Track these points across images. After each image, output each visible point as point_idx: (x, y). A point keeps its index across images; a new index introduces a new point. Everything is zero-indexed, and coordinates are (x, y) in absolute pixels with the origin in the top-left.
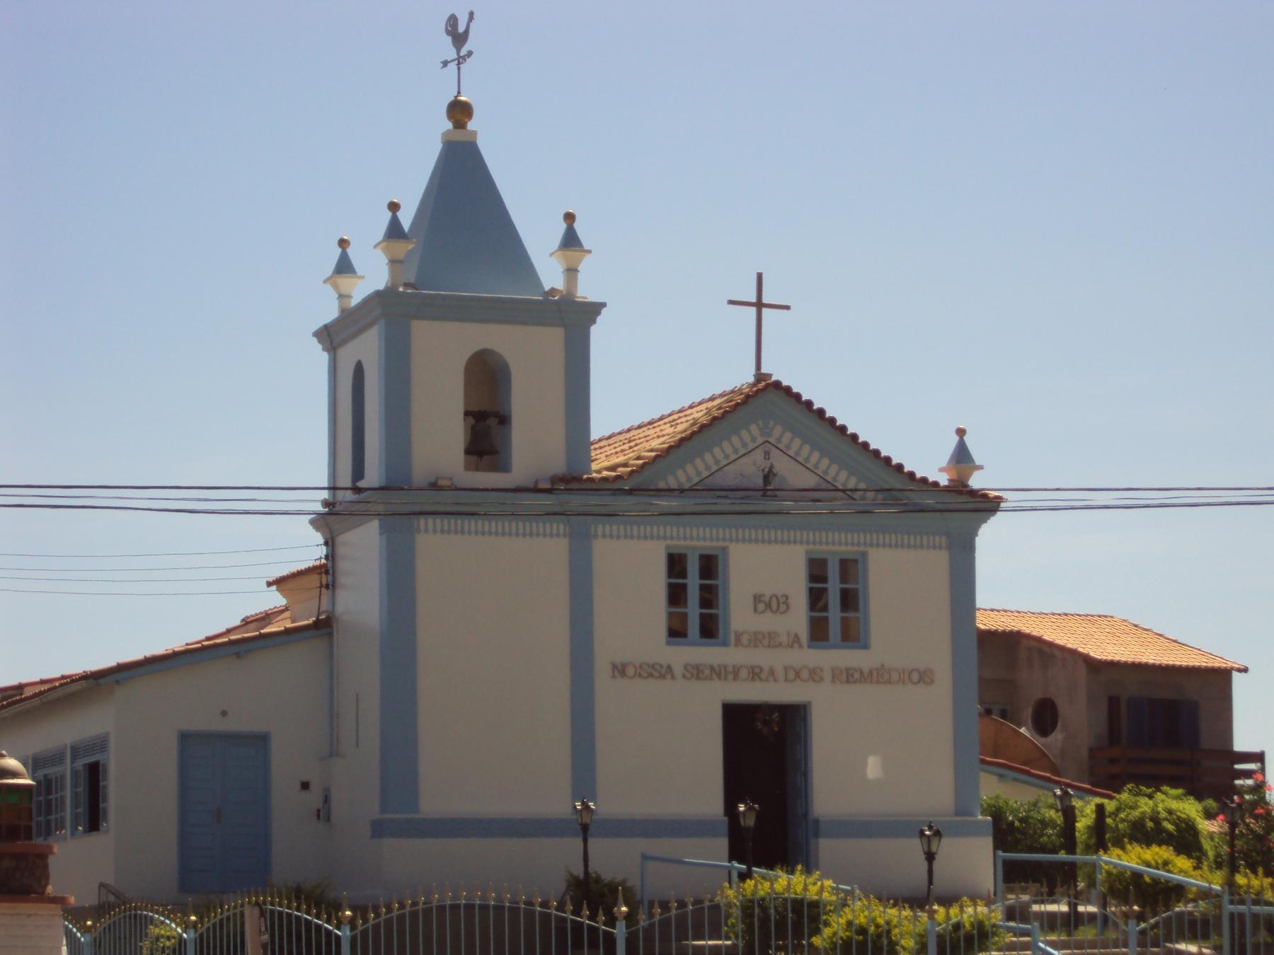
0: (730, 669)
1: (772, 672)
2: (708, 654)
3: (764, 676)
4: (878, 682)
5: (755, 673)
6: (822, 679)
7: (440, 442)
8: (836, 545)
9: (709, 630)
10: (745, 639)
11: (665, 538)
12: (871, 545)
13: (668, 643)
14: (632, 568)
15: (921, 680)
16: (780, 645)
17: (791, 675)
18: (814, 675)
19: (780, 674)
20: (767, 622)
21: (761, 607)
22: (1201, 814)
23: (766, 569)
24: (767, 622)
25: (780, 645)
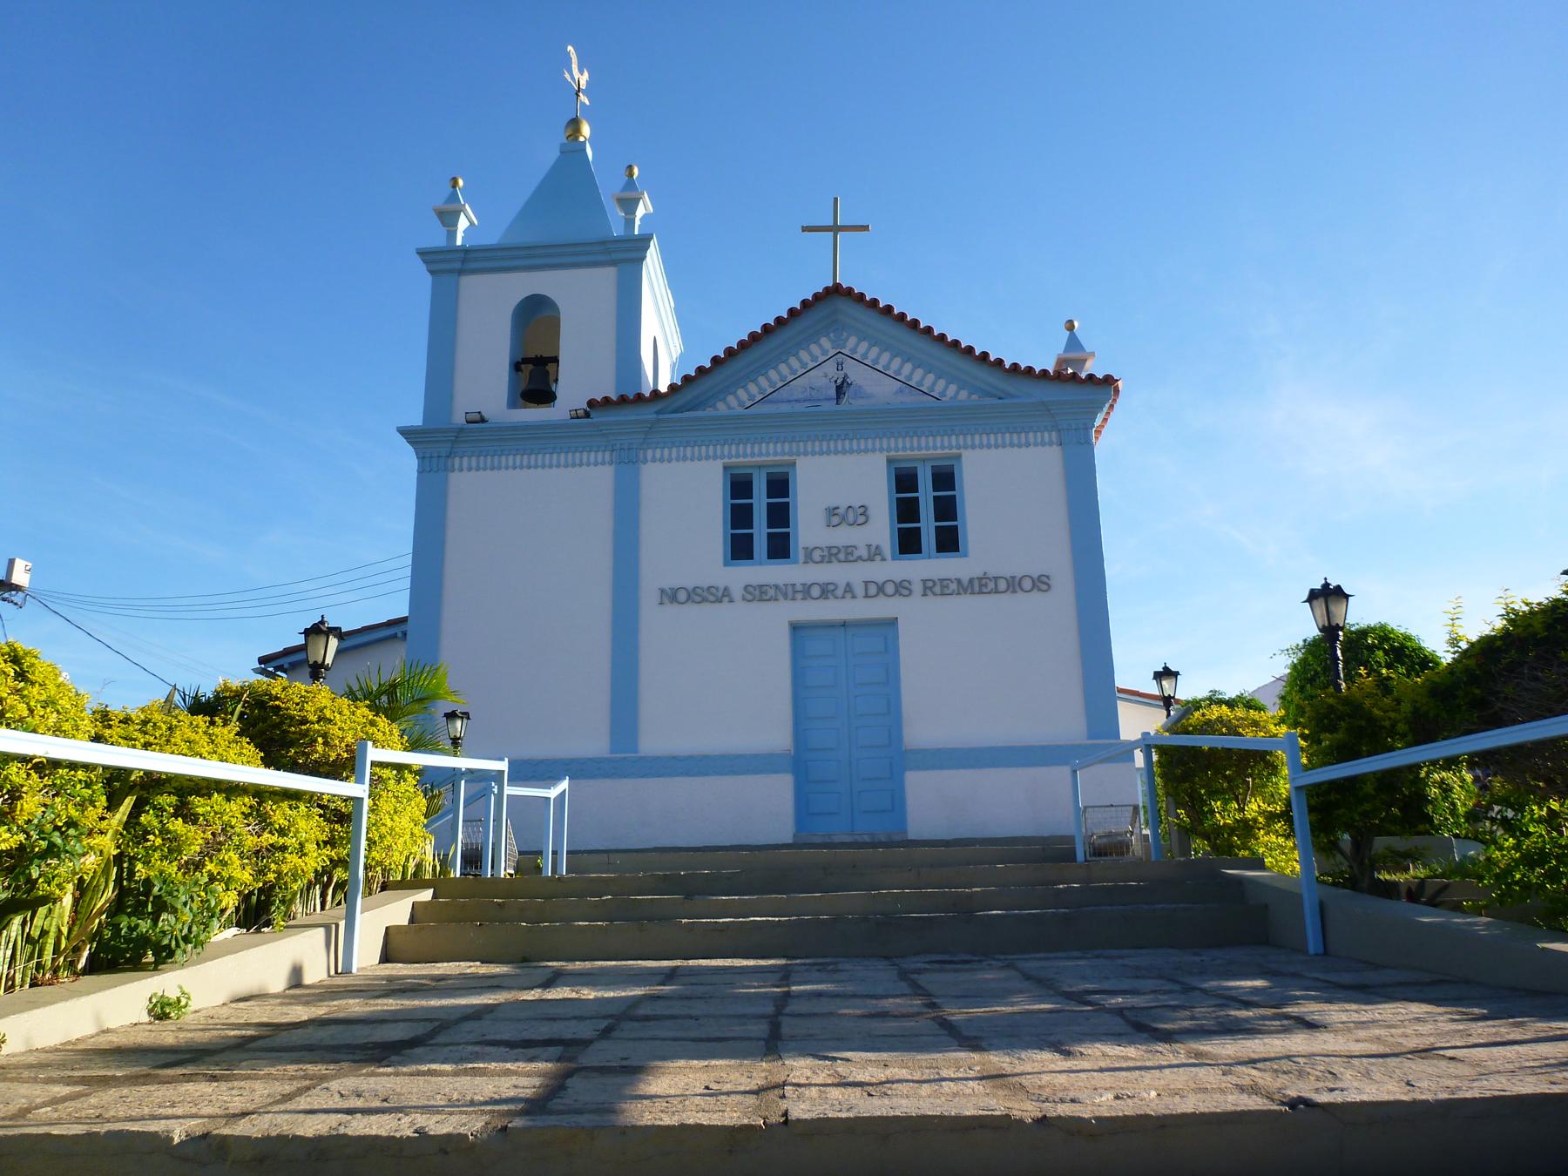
1: (849, 588)
2: (946, 566)
3: (840, 592)
4: (981, 593)
7: (486, 383)
8: (924, 450)
9: (780, 548)
11: (722, 457)
12: (966, 447)
13: (966, 555)
14: (685, 496)
15: (897, 592)
16: (860, 558)
17: (873, 590)
18: (902, 588)
19: (859, 590)
20: (843, 536)
21: (835, 520)
22: (173, 995)
23: (841, 486)
24: (843, 536)
25: (860, 558)
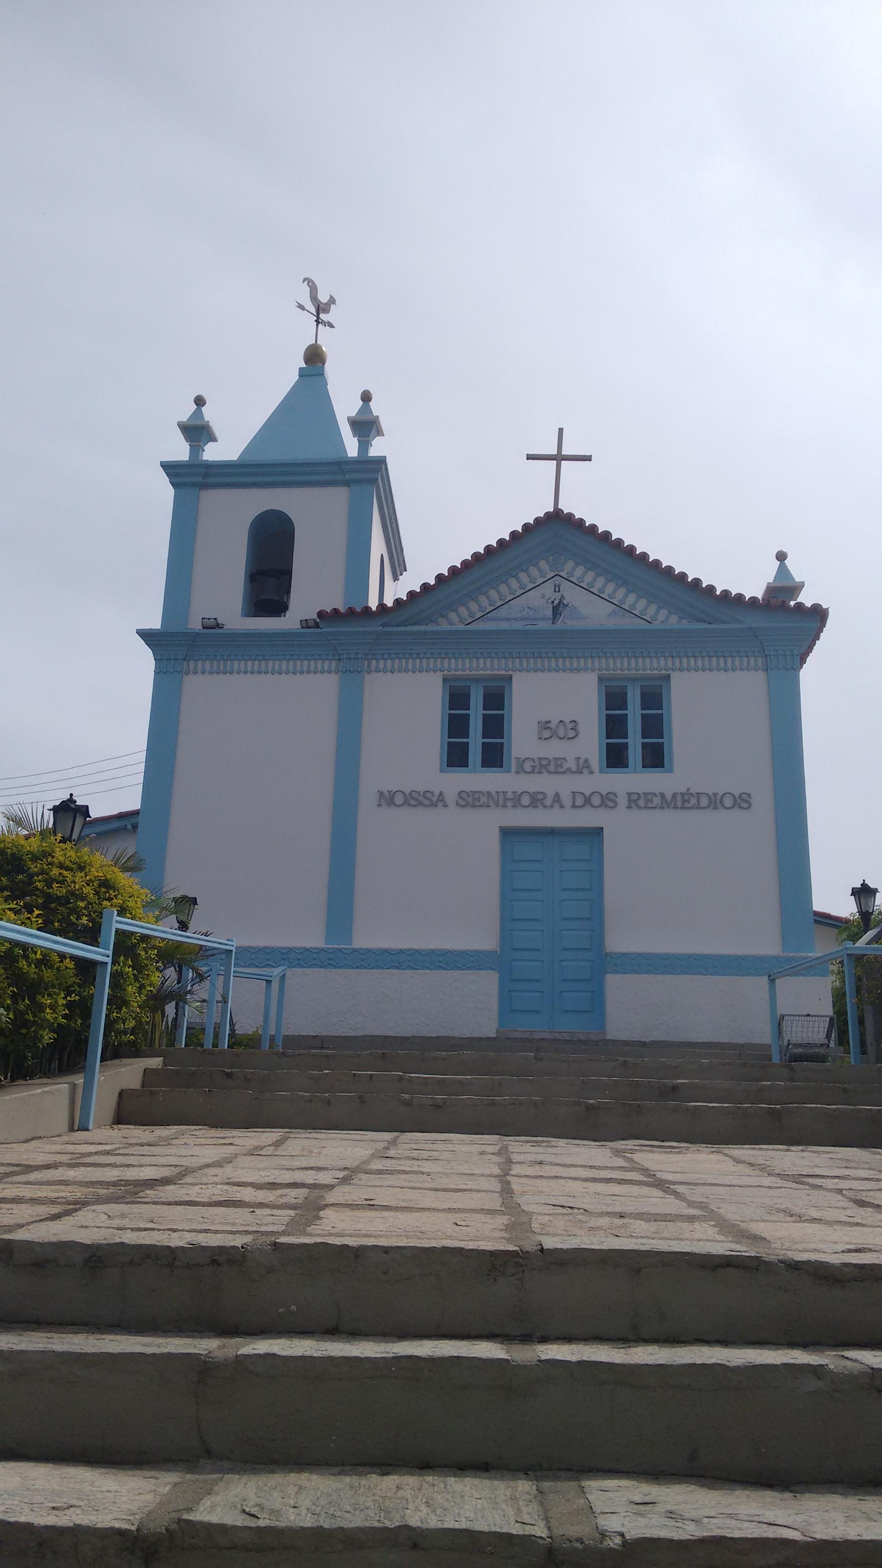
0: (510, 795)
1: (557, 798)
3: (548, 802)
5: (536, 800)
6: (616, 804)
7: (223, 594)
10: (527, 766)
14: (408, 706)
17: (580, 801)
18: (608, 801)
19: (567, 800)
20: (554, 749)
23: (553, 702)
24: (554, 749)
25: (569, 770)
